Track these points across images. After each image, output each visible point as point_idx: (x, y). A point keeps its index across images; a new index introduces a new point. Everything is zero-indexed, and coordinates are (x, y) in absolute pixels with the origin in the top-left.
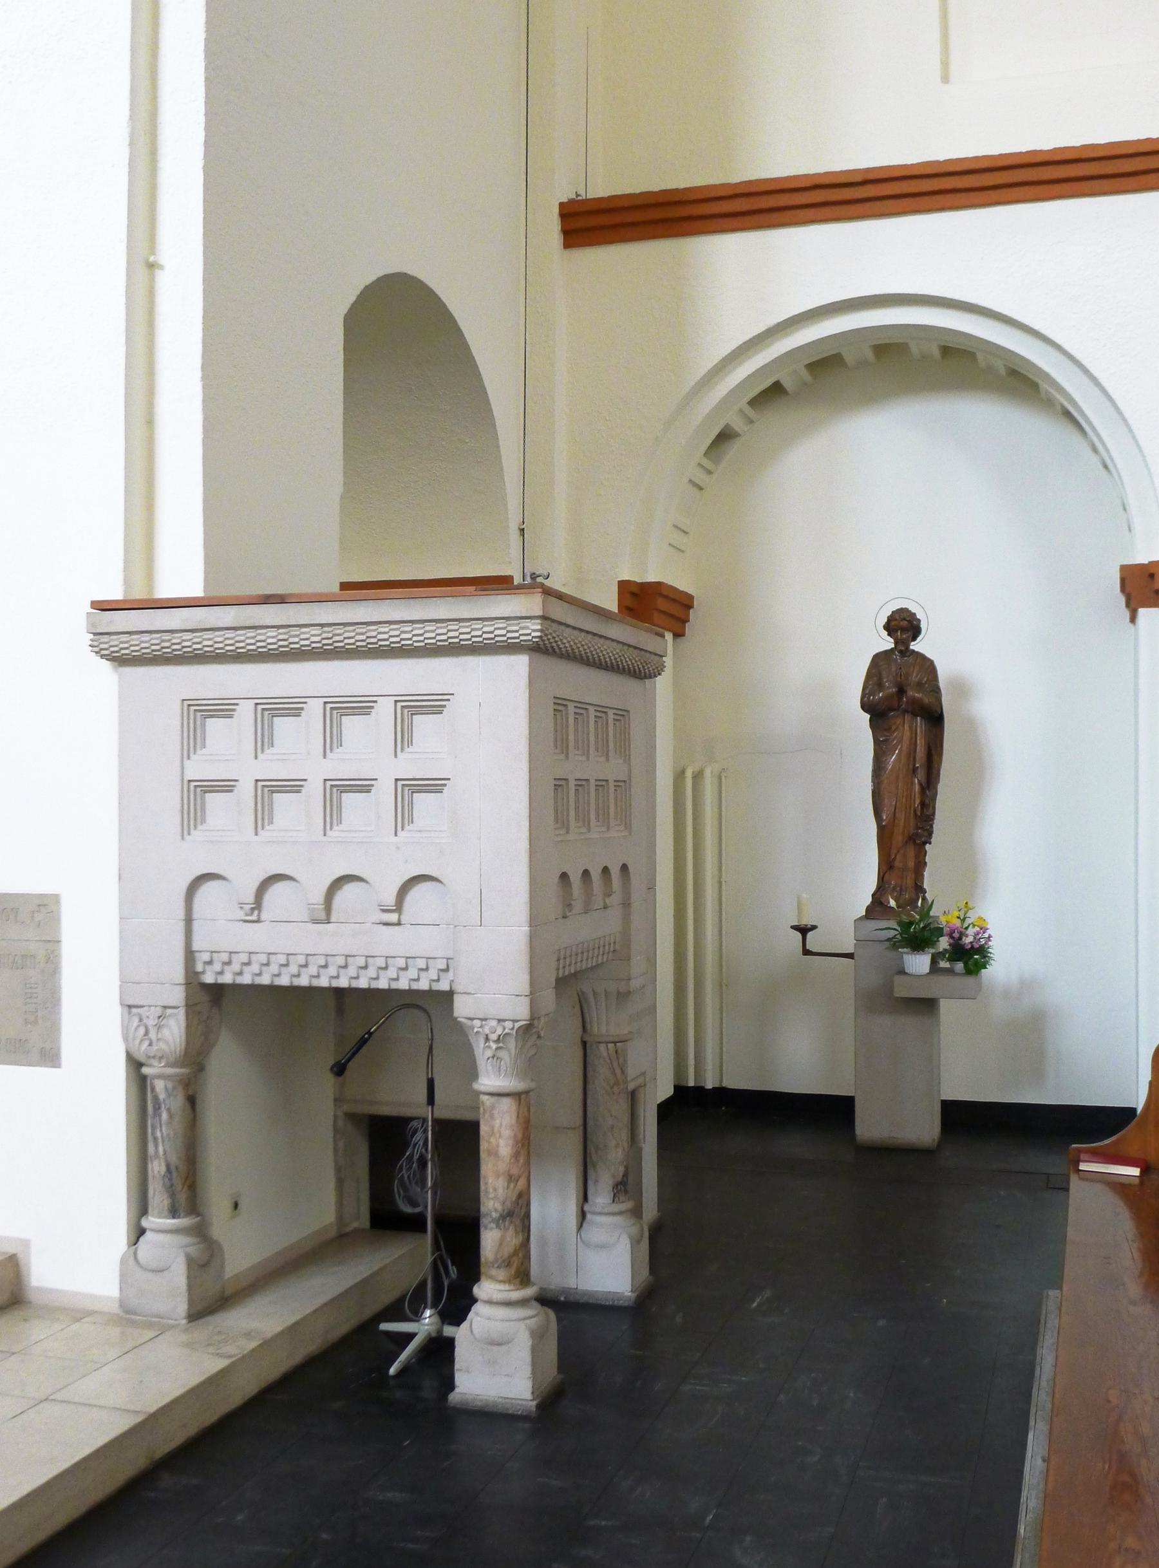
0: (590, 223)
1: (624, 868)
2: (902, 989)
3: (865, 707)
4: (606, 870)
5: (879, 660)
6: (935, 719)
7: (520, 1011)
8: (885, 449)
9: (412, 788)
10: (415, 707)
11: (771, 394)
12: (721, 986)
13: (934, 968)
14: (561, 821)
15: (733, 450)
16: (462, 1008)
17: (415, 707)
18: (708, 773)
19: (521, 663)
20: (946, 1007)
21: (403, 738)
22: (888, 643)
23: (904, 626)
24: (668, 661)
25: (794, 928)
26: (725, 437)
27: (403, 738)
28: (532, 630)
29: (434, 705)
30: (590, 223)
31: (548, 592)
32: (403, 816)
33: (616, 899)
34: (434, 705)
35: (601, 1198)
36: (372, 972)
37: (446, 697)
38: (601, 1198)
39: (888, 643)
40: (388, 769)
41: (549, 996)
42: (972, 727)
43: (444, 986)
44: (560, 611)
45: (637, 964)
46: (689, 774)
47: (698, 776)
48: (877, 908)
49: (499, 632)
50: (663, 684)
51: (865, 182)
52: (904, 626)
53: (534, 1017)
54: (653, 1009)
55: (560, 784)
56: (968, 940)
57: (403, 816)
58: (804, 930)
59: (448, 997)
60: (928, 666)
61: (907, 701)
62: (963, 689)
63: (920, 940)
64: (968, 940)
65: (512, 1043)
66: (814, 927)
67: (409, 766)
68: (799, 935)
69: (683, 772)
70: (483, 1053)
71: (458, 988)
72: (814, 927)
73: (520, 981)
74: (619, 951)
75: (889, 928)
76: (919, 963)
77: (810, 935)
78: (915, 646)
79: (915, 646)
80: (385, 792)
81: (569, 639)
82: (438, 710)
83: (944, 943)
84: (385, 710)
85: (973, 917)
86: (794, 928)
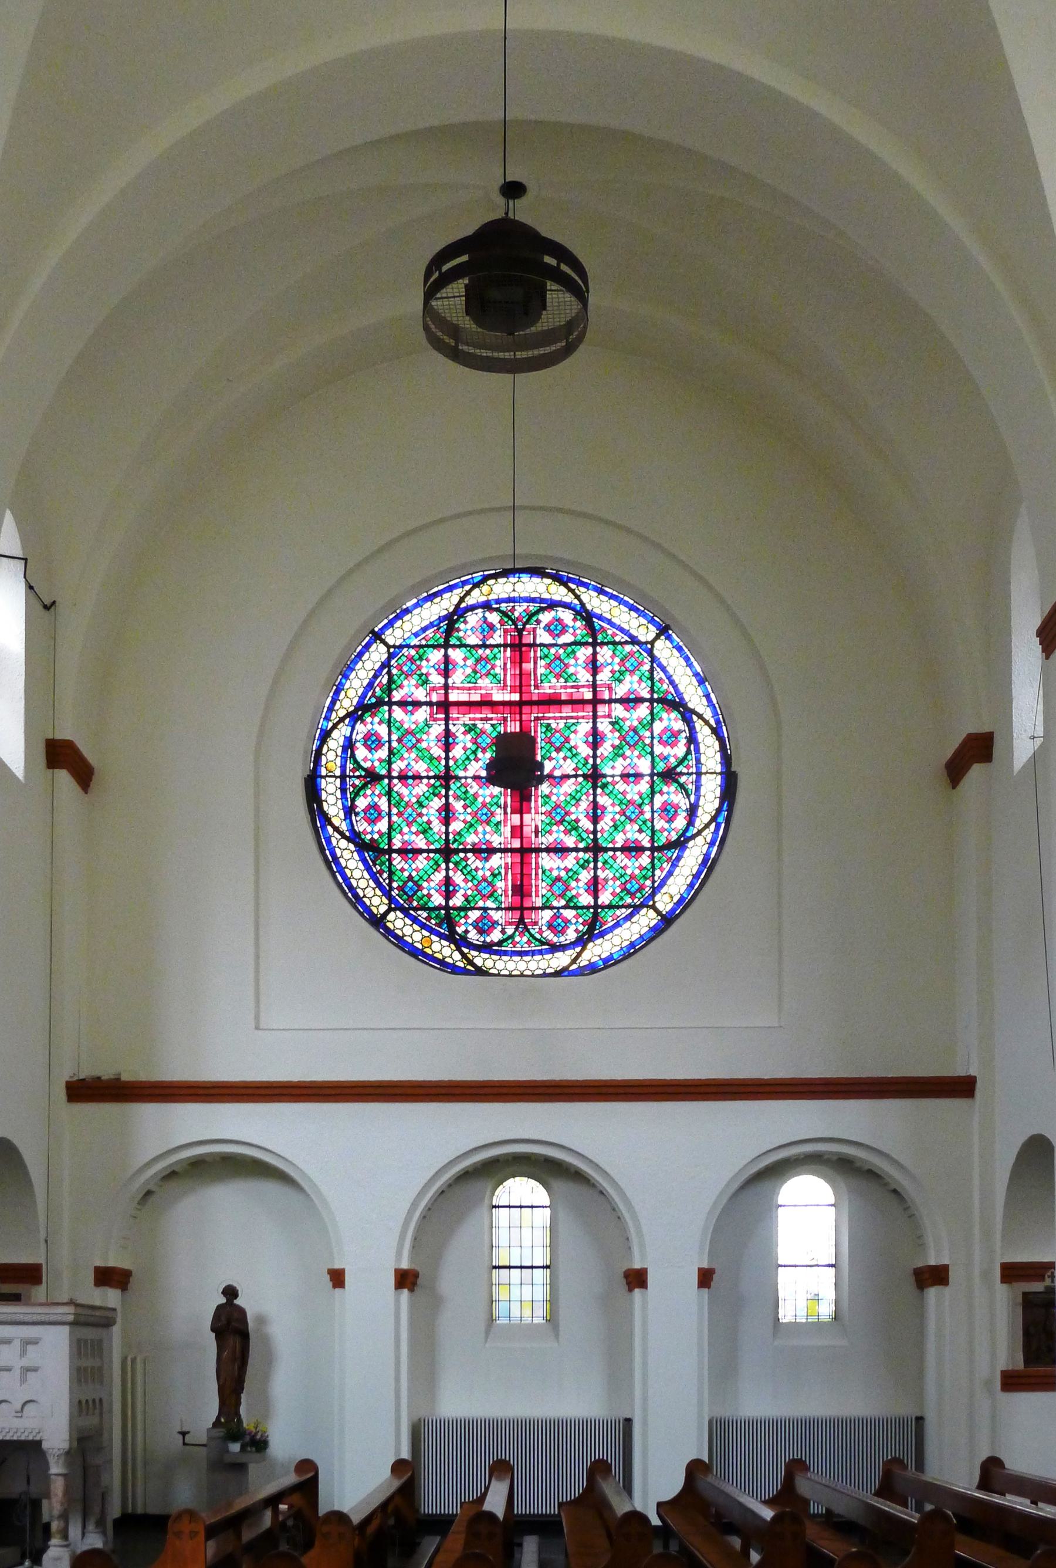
0: (84, 1091)
1: (101, 1400)
2: (228, 1459)
3: (213, 1330)
4: (94, 1401)
5: (220, 1308)
6: (244, 1335)
7: (66, 1445)
8: (226, 1201)
9: (27, 1370)
10: (27, 1342)
11: (171, 1175)
12: (145, 1463)
13: (243, 1448)
14: (79, 1381)
15: (152, 1199)
16: (45, 1445)
17: (27, 1342)
18: (138, 1359)
19: (66, 1329)
20: (252, 1468)
21: (23, 1353)
22: (223, 1300)
23: (230, 1292)
24: (119, 1320)
25: (180, 1433)
26: (149, 1193)
27: (23, 1353)
28: (71, 1318)
29: (35, 1342)
30: (84, 1091)
31: (77, 1305)
32: (23, 1380)
33: (97, 1411)
34: (35, 1342)
35: (91, 1527)
36: (11, 1434)
37: (40, 1339)
38: (91, 1527)
39: (223, 1300)
40: (18, 1363)
41: (75, 1444)
42: (266, 1340)
43: (38, 1438)
44: (80, 1311)
45: (106, 1436)
46: (129, 1359)
47: (134, 1361)
48: (217, 1424)
49: (59, 1318)
50: (116, 1329)
51: (214, 1087)
52: (230, 1292)
53: (70, 1448)
54: (111, 1461)
55: (79, 1369)
56: (258, 1437)
57: (23, 1380)
58: (184, 1434)
59: (39, 1443)
60: (242, 1312)
61: (232, 1326)
62: (262, 1320)
63: (237, 1437)
64: (258, 1437)
65: (63, 1458)
66: (188, 1432)
67: (25, 1362)
68: (181, 1437)
69: (126, 1358)
70: (52, 1461)
71: (45, 1437)
72: (188, 1432)
73: (66, 1435)
74: (99, 1431)
75: (220, 1432)
76: (235, 1447)
77: (187, 1437)
78: (236, 1302)
79: (236, 1302)
80: (17, 1372)
81: (82, 1319)
82: (36, 1343)
83: (247, 1438)
84: (17, 1343)
85: (260, 1428)
86: (180, 1433)
